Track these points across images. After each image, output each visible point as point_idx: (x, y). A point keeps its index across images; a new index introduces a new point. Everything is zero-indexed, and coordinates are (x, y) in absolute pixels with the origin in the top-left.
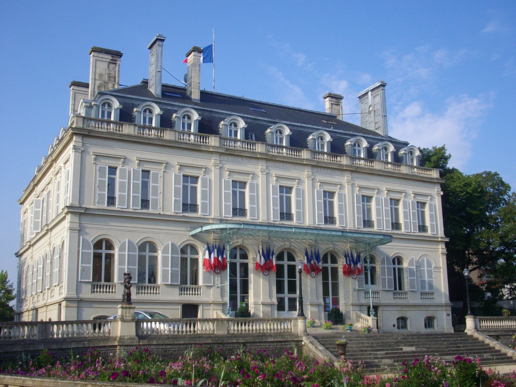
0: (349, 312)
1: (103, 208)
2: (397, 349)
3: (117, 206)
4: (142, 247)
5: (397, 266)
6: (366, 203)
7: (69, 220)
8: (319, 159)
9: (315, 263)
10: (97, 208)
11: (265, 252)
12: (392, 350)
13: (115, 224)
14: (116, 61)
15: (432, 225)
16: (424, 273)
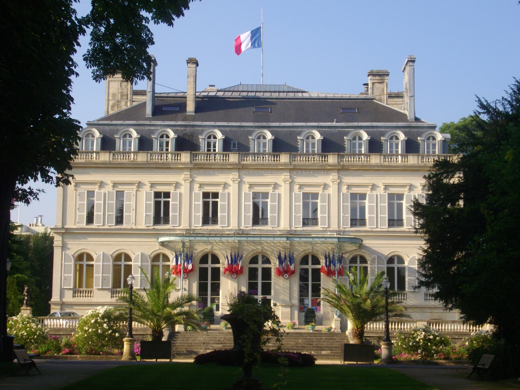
1: (82, 227)
4: (118, 258)
11: (233, 257)
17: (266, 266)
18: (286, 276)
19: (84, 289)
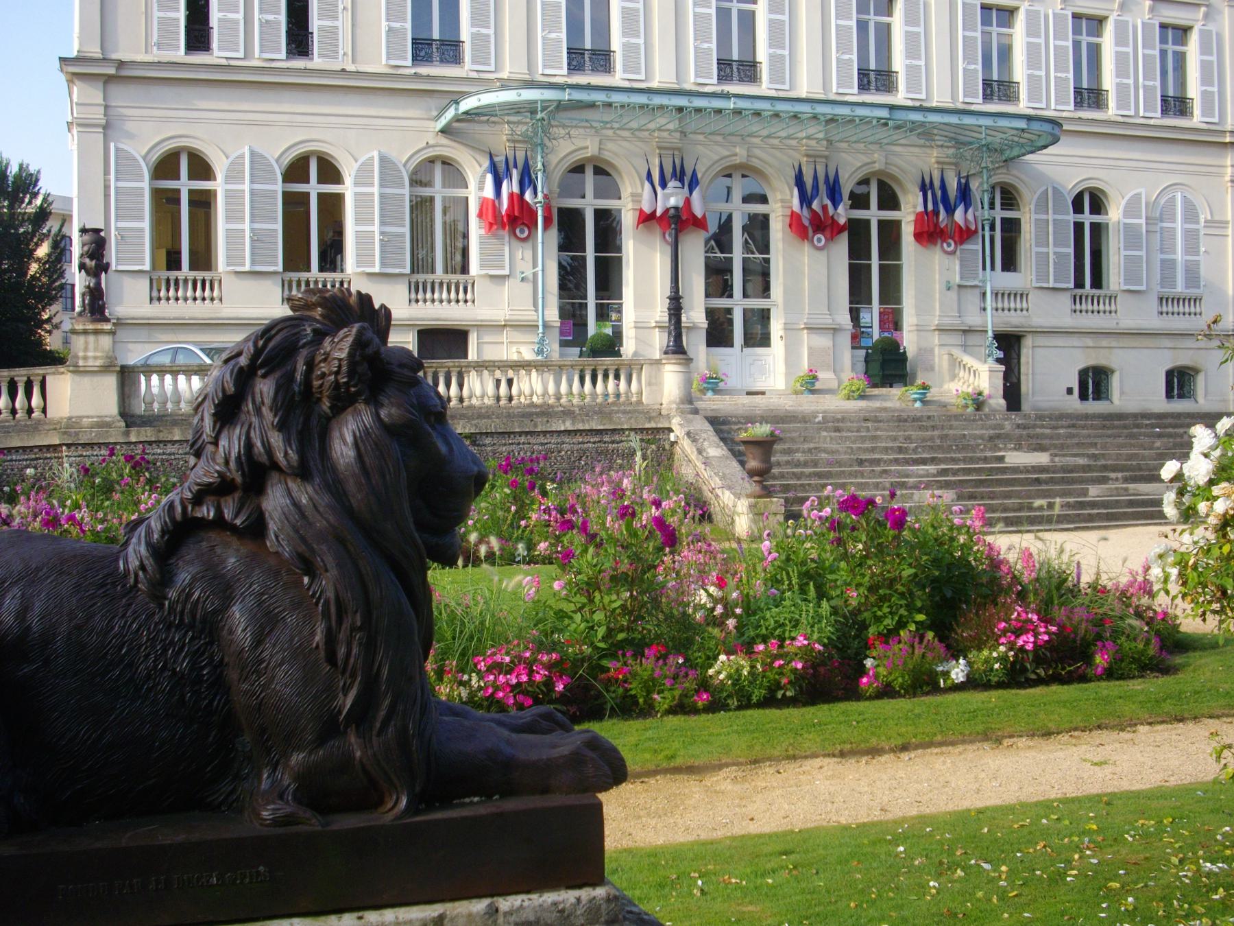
0: (932, 350)
2: (985, 460)
3: (217, 54)
4: (296, 170)
5: (1087, 218)
6: (995, 29)
9: (825, 208)
10: (156, 60)
12: (964, 460)
15: (1206, 96)
16: (1174, 238)
18: (819, 240)
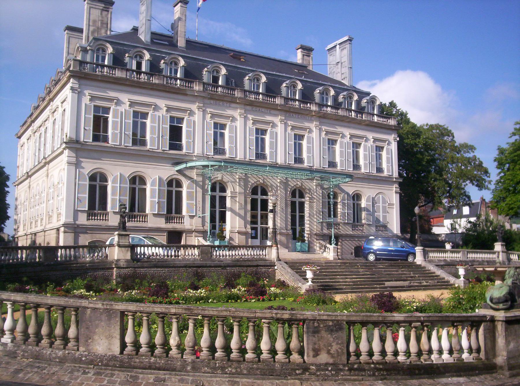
4: (170, 183)
7: (67, 155)
8: (171, 84)
13: (365, 185)
14: (108, 8)
17: (264, 197)
19: (136, 213)
